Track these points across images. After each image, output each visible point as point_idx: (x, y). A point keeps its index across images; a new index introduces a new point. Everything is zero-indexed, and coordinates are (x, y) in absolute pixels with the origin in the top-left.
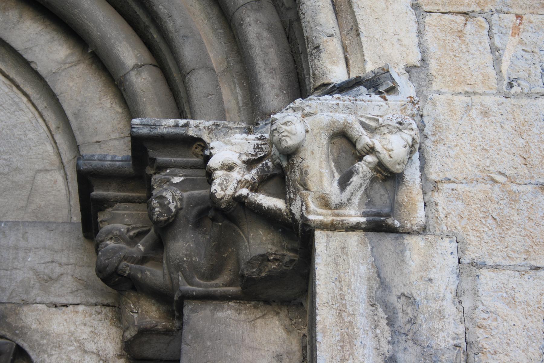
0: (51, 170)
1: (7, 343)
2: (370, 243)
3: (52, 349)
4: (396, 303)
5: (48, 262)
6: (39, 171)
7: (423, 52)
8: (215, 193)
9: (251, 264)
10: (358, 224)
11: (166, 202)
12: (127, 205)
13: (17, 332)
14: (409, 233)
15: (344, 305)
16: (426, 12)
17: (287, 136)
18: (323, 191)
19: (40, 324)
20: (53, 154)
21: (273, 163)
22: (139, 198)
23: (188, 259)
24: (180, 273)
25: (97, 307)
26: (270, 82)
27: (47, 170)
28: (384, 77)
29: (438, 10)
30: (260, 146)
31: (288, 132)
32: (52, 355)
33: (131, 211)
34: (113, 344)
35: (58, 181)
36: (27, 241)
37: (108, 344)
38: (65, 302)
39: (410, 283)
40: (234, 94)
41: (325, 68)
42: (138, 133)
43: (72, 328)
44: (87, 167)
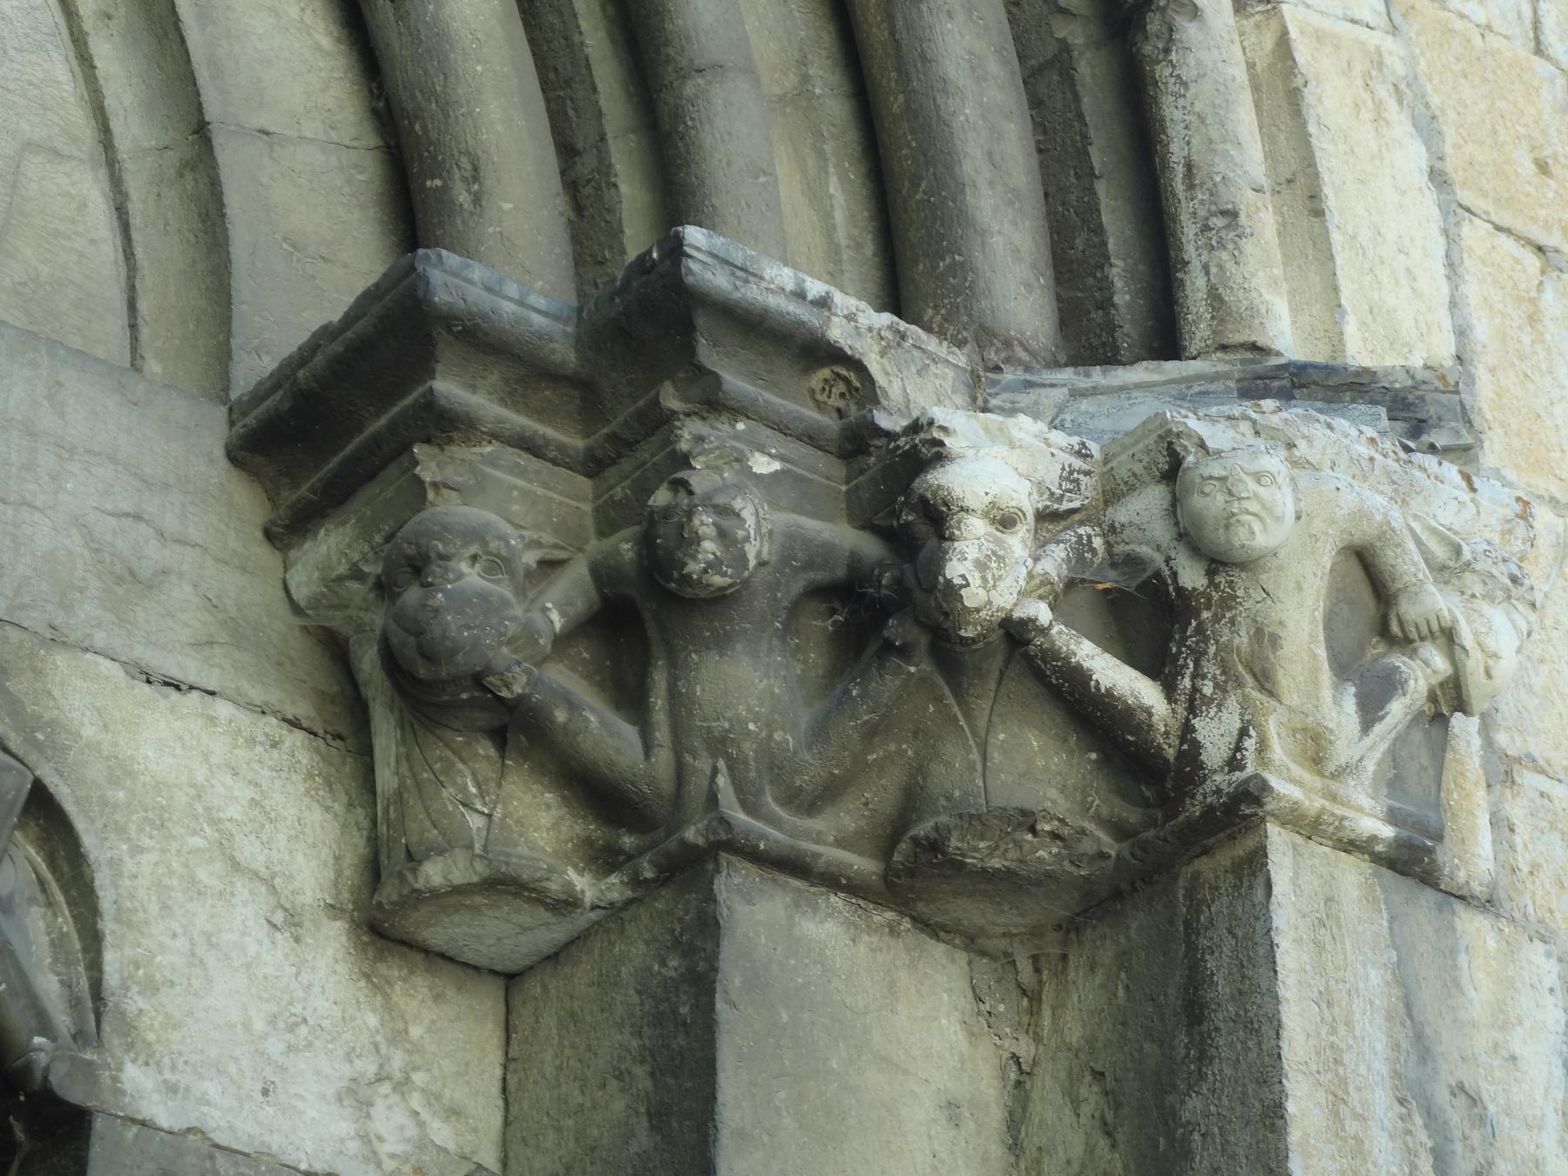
0: (70, 158)
1: (10, 768)
2: (1386, 904)
3: (141, 830)
4: (1450, 1109)
5: (127, 515)
6: (31, 146)
7: (1462, 333)
8: (962, 586)
9: (984, 825)
10: (1374, 839)
11: (741, 534)
12: (523, 459)
13: (40, 736)
14: (1462, 898)
15: (1343, 1081)
16: (1460, 205)
17: (1255, 515)
18: (1319, 717)
19: (106, 727)
20: (72, 100)
21: (1109, 546)
22: (561, 448)
23: (761, 731)
24: (721, 764)
25: (265, 719)
26: (1006, 232)
27: (56, 153)
28: (1439, 402)
29: (1485, 212)
30: (1075, 475)
31: (1264, 506)
32: (142, 850)
33: (530, 481)
34: (314, 863)
35: (90, 205)
36: (62, 415)
37: (300, 858)
38: (176, 674)
39: (1473, 1054)
40: (817, 196)
41: (1254, 294)
42: (703, 279)
43: (200, 775)
44: (450, 300)
